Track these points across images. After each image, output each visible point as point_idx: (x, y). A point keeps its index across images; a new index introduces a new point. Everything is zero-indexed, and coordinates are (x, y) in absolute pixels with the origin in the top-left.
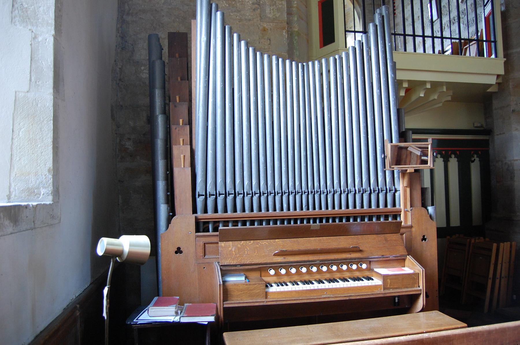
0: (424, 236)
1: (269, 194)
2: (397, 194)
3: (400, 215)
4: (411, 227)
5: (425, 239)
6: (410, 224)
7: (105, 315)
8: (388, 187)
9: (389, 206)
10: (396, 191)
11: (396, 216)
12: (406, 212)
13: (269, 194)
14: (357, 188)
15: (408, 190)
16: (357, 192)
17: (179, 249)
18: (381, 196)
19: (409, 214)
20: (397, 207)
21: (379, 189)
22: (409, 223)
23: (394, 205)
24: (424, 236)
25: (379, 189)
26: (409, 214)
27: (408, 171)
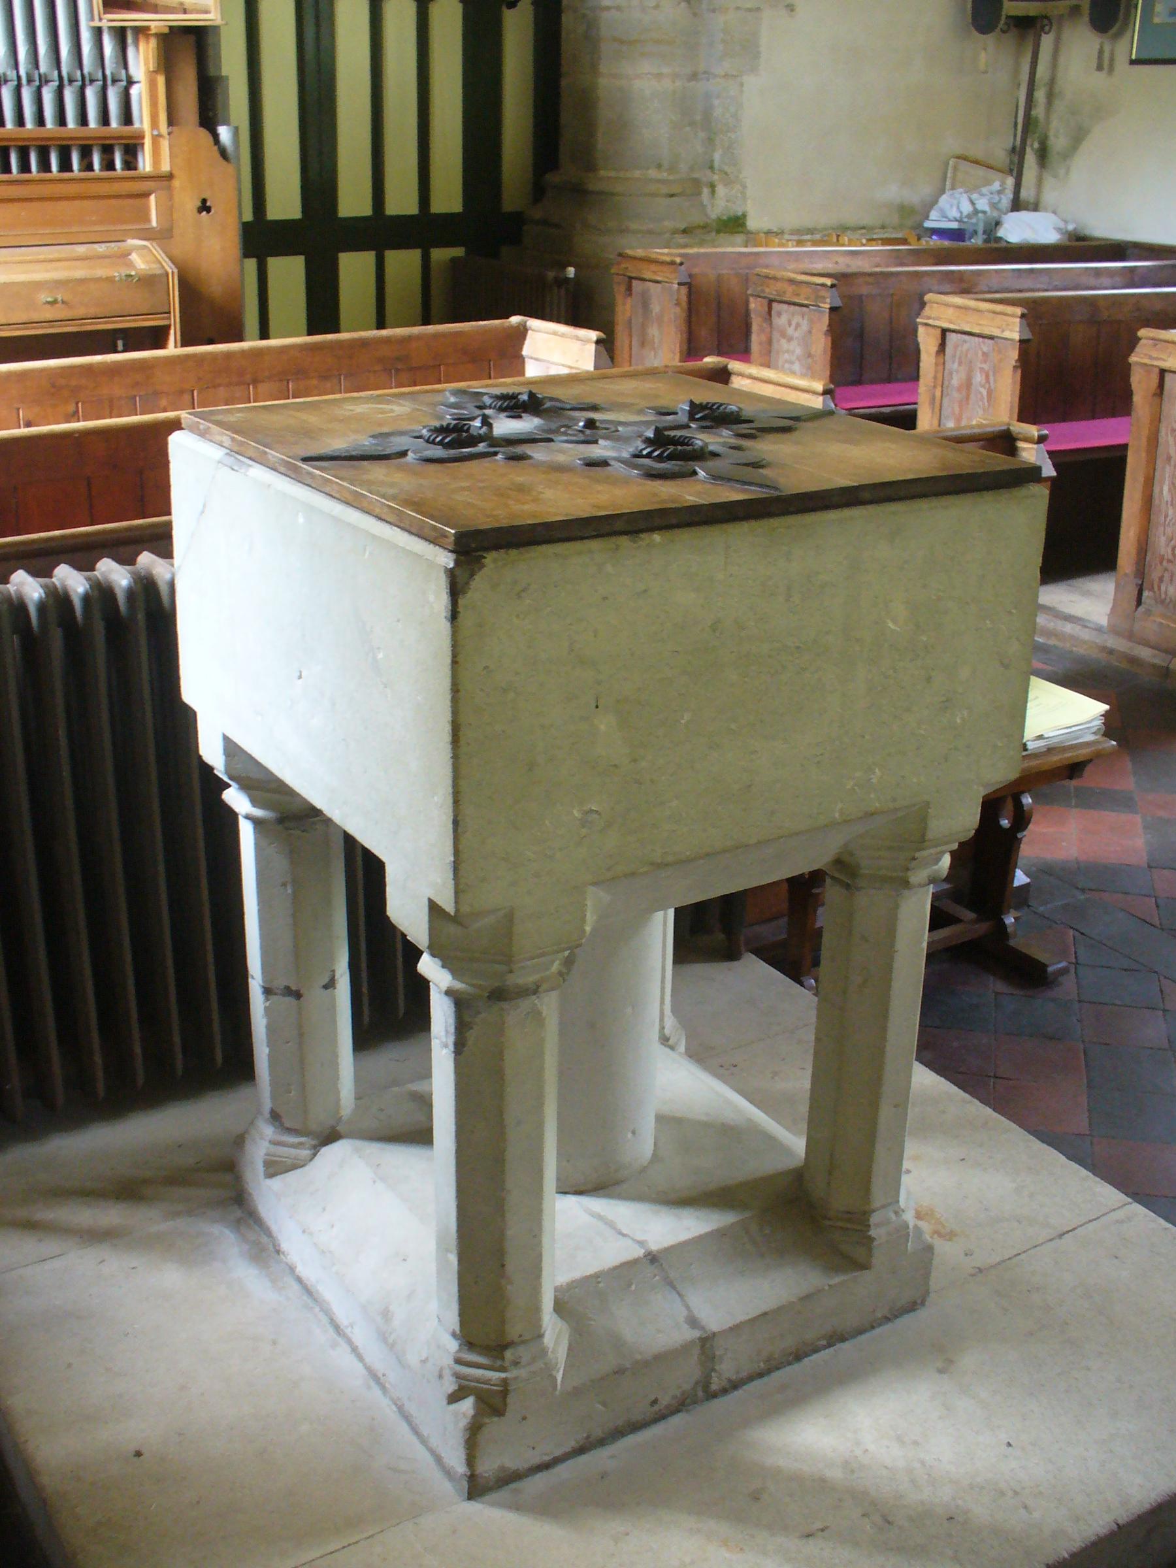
0: (204, 201)
1: (44, 80)
2: (134, 91)
3: (143, 144)
4: (170, 177)
5: (208, 210)
6: (168, 169)
7: (707, 360)
8: (108, 72)
9: (114, 124)
10: (131, 82)
11: (132, 151)
12: (156, 139)
13: (44, 80)
14: (22, 73)
15: (161, 80)
16: (24, 81)
17: (208, 210)
18: (91, 94)
19: (165, 144)
20: (137, 125)
21: (83, 76)
22: (165, 167)
23: (127, 118)
24: (204, 201)
25: (83, 76)
26: (165, 144)
27: (153, 31)
